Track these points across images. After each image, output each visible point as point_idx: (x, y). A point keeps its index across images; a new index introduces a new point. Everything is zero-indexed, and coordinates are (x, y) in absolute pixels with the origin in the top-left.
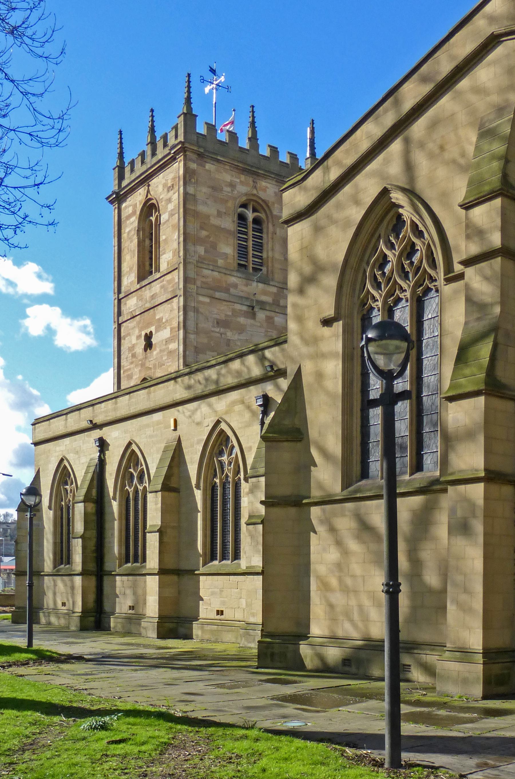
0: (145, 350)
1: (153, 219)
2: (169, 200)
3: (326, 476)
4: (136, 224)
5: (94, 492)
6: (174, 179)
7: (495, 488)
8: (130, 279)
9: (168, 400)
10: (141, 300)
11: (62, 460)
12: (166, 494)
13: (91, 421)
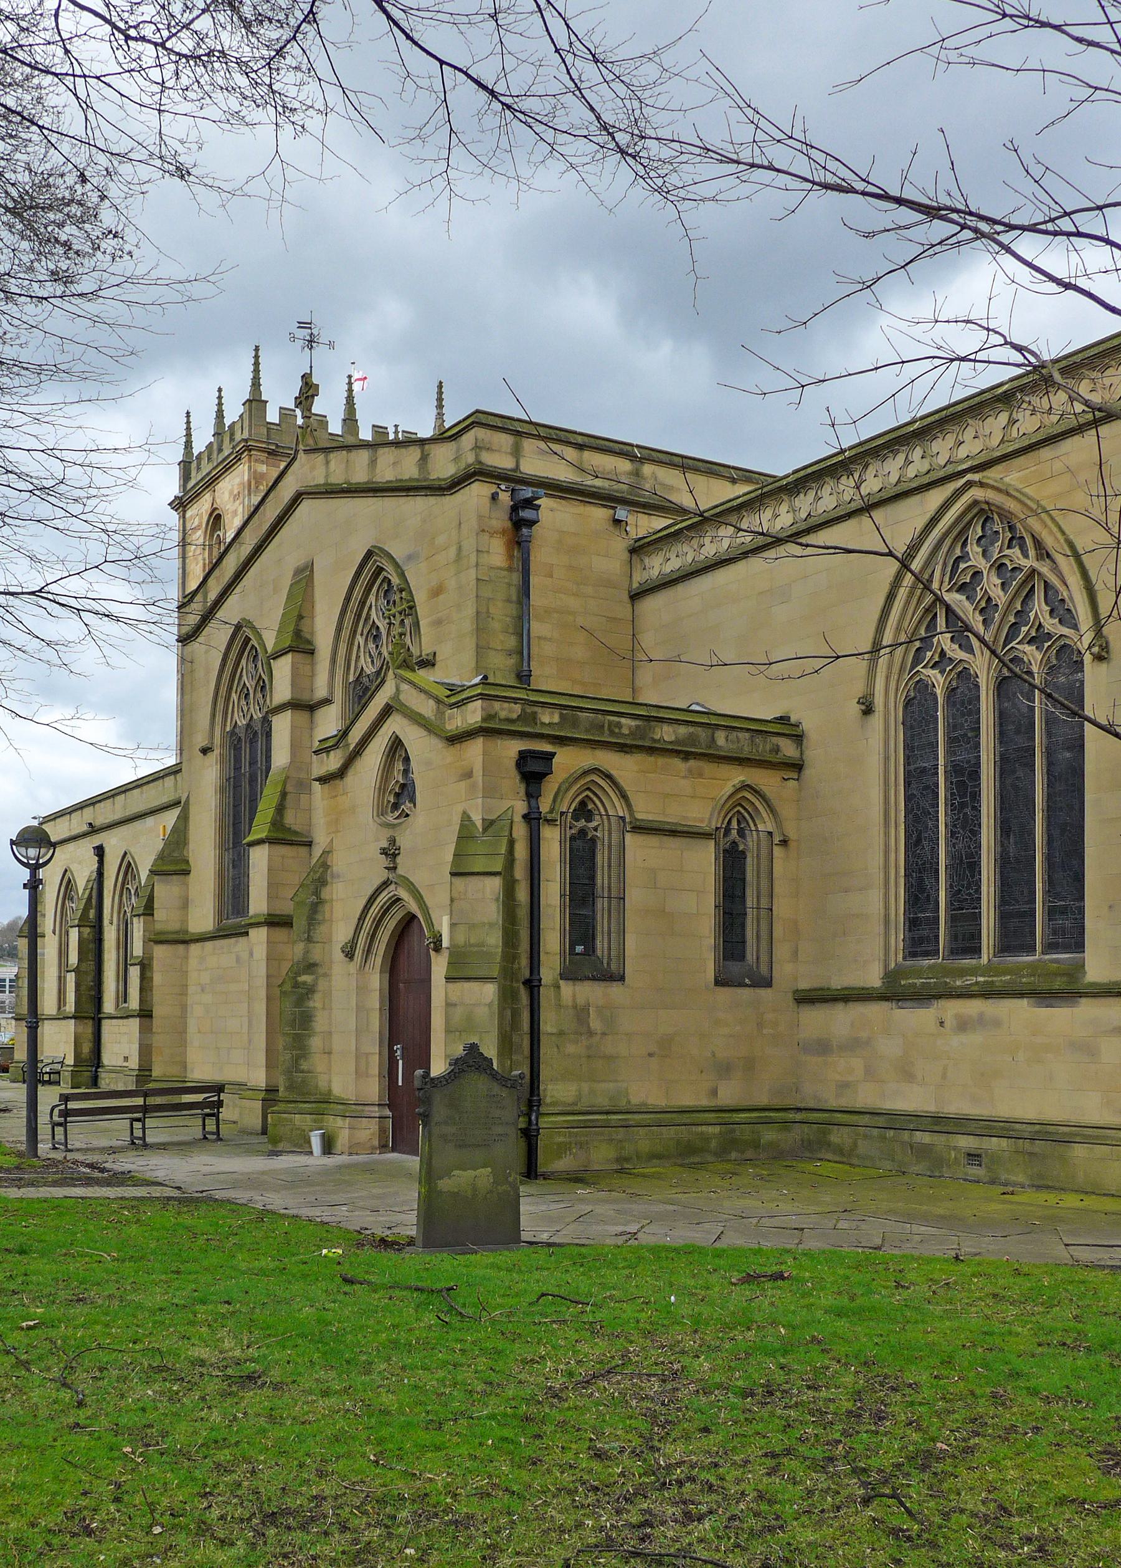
5: (92, 913)
9: (118, 815)
13: (90, 824)
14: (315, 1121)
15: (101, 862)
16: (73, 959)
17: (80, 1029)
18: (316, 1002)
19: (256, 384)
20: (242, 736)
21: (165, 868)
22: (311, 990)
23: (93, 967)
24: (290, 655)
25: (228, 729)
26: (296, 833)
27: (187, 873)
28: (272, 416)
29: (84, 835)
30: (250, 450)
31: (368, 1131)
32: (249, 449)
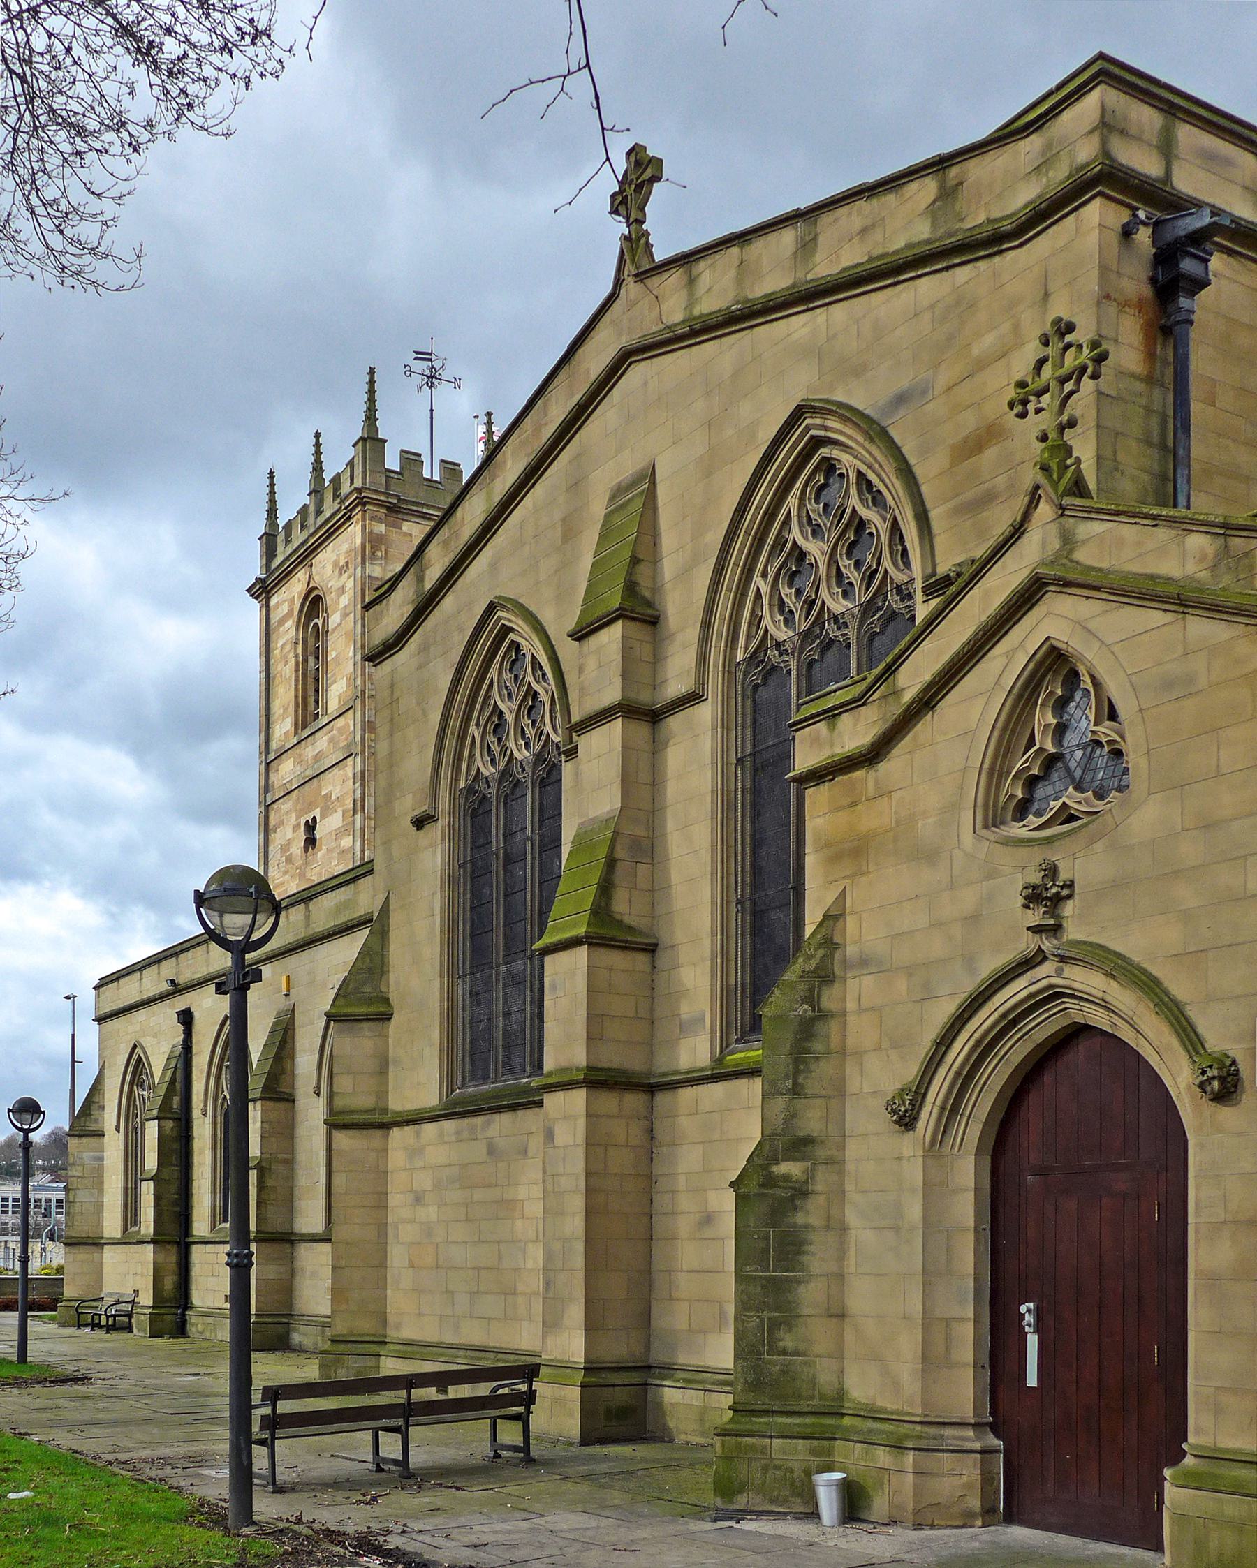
0: (306, 849)
1: (320, 623)
2: (342, 590)
3: (419, 1080)
4: (293, 632)
6: (349, 552)
7: (609, 1101)
8: (283, 728)
10: (300, 763)
11: (135, 1046)
12: (270, 1104)
13: (172, 981)
14: (814, 1452)
15: (188, 1033)
16: (151, 1162)
17: (161, 1258)
18: (810, 1215)
19: (371, 417)
20: (492, 792)
21: (350, 1010)
22: (799, 1193)
23: (177, 1175)
24: (619, 625)
25: (462, 784)
26: (630, 929)
27: (386, 1017)
28: (392, 462)
29: (162, 997)
30: (364, 504)
31: (960, 1478)
32: (362, 502)
